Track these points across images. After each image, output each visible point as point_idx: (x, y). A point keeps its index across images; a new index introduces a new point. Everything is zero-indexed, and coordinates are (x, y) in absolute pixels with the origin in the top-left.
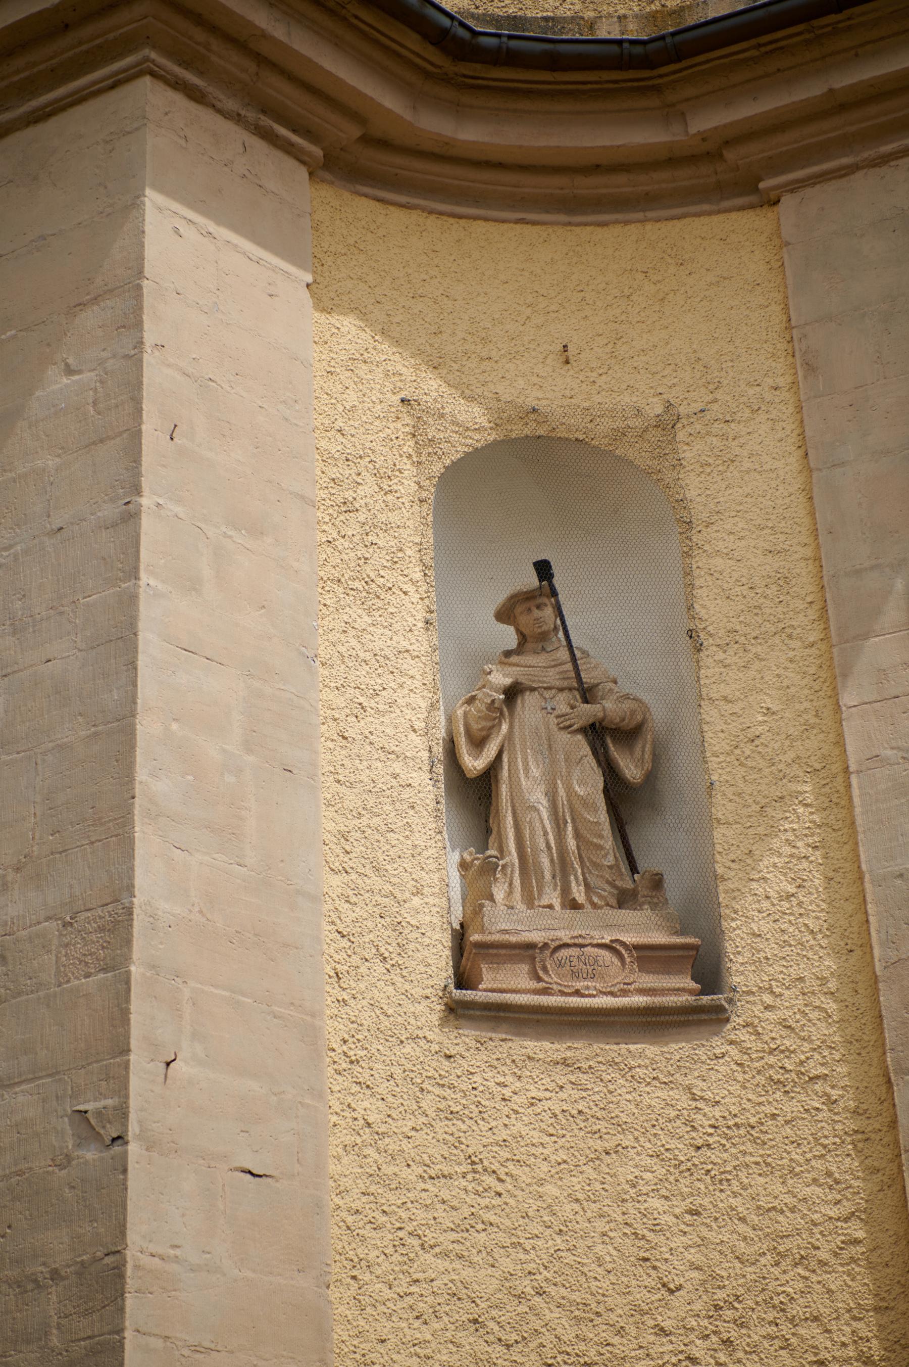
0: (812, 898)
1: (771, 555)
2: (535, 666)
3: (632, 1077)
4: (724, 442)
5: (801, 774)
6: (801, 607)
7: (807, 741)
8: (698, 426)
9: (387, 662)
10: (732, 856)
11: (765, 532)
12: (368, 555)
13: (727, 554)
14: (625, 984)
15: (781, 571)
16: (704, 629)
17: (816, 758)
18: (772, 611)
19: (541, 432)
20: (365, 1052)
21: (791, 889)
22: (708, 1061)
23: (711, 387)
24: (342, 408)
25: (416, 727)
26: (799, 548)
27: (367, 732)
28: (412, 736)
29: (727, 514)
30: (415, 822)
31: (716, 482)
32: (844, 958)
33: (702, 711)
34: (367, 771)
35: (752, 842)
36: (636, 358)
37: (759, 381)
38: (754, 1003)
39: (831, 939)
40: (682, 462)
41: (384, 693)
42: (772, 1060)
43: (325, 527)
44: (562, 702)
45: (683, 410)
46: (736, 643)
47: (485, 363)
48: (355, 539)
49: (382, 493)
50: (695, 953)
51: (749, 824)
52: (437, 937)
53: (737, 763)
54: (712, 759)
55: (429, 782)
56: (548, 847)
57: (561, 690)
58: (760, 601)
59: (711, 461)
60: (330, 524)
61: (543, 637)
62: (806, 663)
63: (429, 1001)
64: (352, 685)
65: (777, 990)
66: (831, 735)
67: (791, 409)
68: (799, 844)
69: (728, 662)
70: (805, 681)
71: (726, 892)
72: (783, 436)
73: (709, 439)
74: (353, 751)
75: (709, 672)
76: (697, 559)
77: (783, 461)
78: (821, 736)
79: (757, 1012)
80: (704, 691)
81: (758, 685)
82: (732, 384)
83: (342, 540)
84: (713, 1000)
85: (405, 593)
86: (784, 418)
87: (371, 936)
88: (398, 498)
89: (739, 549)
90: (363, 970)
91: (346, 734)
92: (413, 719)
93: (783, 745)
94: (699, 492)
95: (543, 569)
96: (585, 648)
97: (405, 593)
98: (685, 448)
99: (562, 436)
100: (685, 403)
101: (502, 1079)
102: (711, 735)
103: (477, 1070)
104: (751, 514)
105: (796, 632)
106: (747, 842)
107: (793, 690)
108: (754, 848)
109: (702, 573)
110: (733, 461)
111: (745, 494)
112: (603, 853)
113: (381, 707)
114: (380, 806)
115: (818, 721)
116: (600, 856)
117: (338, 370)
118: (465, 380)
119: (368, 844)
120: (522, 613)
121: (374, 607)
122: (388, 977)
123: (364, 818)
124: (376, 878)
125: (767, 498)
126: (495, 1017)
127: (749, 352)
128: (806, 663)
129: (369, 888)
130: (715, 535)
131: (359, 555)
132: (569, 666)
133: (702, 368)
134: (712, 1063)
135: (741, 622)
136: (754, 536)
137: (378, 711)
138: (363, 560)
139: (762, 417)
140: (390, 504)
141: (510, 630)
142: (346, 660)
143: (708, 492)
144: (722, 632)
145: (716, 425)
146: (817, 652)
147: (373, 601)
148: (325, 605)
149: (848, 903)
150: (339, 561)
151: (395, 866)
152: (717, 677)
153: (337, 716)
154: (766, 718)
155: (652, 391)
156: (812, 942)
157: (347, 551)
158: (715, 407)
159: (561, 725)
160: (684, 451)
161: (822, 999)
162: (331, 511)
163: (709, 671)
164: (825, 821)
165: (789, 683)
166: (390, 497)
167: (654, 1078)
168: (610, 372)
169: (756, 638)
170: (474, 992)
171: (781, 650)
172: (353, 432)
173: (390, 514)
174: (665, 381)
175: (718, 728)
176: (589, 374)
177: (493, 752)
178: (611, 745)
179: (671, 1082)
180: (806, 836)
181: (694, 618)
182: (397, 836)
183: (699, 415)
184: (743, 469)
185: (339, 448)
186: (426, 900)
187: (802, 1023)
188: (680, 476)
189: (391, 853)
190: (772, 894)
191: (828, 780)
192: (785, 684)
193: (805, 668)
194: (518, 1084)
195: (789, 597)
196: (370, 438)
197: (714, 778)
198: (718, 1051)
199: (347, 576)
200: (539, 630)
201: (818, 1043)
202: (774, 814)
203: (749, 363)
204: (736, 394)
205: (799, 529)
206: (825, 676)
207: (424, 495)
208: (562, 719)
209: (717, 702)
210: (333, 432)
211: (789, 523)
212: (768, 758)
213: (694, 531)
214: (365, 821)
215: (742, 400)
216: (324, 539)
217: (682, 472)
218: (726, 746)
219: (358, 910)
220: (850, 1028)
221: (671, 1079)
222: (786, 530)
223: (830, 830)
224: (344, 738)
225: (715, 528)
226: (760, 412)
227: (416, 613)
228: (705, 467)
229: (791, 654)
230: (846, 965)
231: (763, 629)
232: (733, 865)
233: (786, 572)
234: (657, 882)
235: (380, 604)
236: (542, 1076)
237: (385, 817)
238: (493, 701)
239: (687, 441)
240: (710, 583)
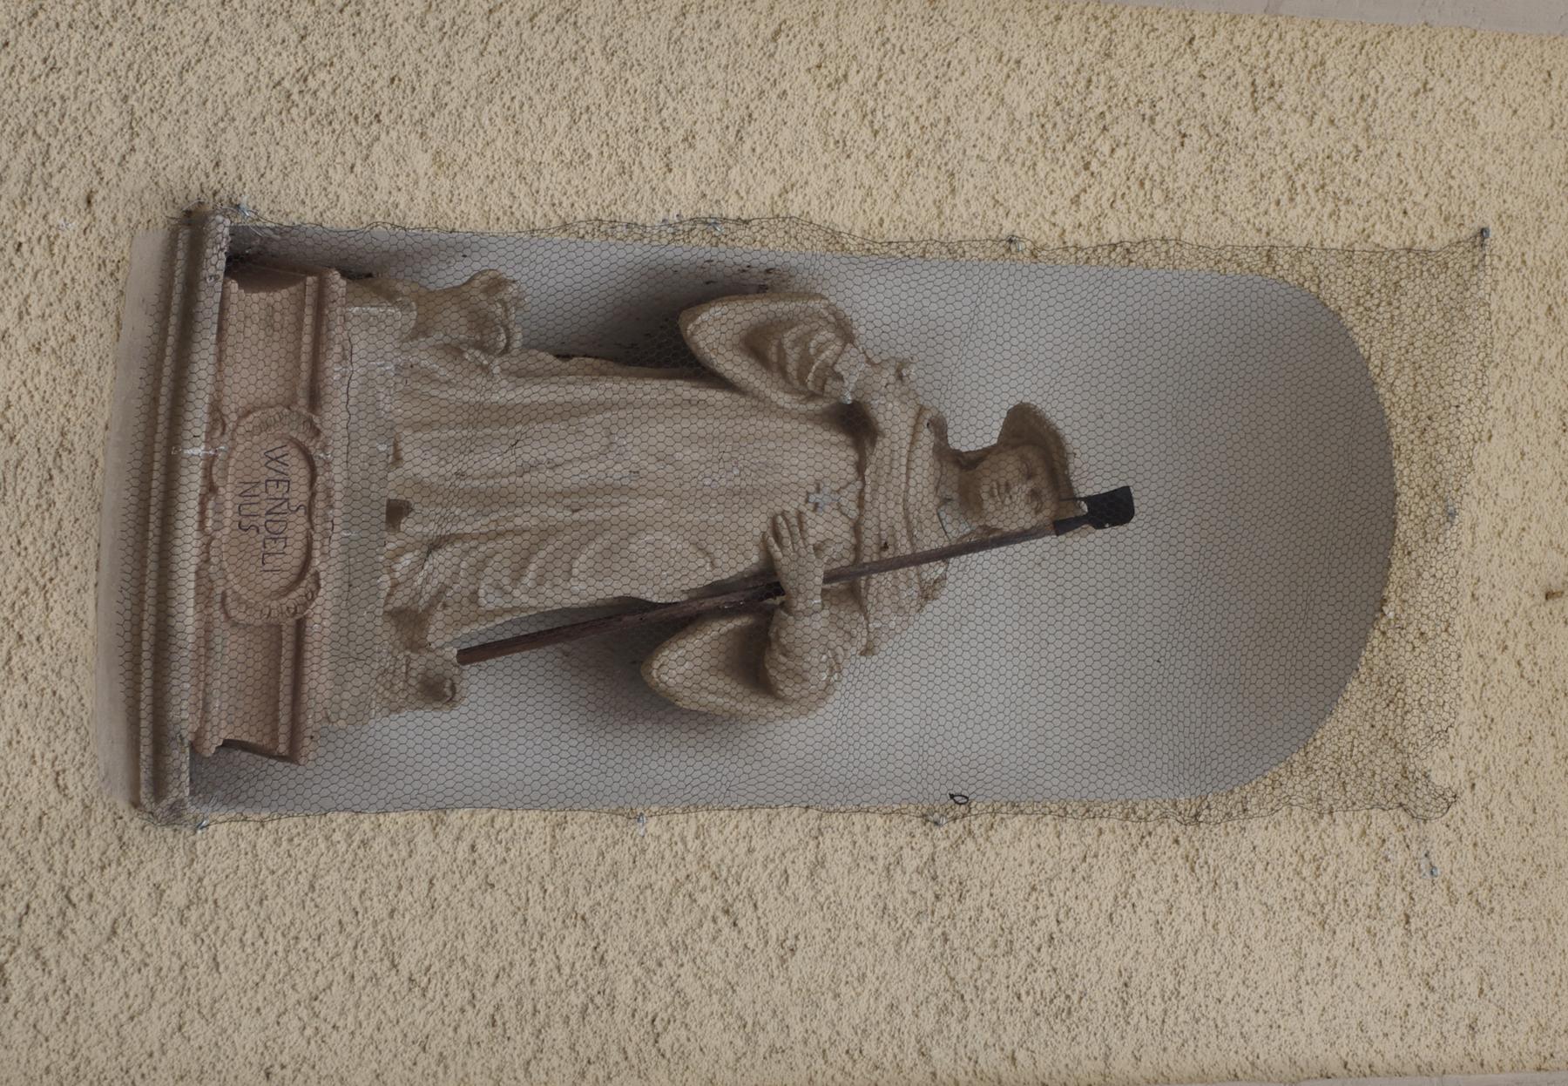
0: (387, 1006)
1: (1120, 985)
2: (907, 482)
3: (26, 592)
4: (1364, 911)
5: (650, 1007)
6: (1005, 1038)
7: (720, 1025)
8: (1400, 859)
9: (932, 145)
10: (483, 846)
11: (1170, 978)
12: (1159, 125)
13: (1126, 894)
14: (224, 595)
15: (1084, 1003)
16: (970, 832)
17: (683, 1040)
18: (1000, 976)
19: (1405, 526)
20: (107, 14)
21: (407, 963)
22: (49, 756)
23: (1483, 894)
24: (1472, 97)
25: (791, 196)
26: (1130, 1043)
27: (785, 85)
28: (773, 186)
29: (1211, 902)
30: (589, 175)
31: (1280, 885)
32: (255, 1059)
33: (796, 811)
34: (703, 80)
35: (512, 890)
36: (1552, 741)
37: (1490, 994)
38: (169, 864)
39: (296, 1034)
40: (1327, 818)
41: (866, 133)
42: (47, 888)
43: (1222, 33)
44: (829, 529)
45: (1436, 828)
46: (937, 897)
47: (1554, 418)
48: (1194, 99)
49: (1290, 168)
50: (282, 749)
51: (550, 889)
52: (344, 196)
53: (681, 875)
54: (693, 822)
55: (674, 212)
56: (525, 470)
57: (856, 529)
58: (1023, 953)
59: (1325, 878)
60: (1228, 46)
61: (968, 500)
62: (886, 1038)
63: (210, 166)
64: (887, 64)
65: (193, 915)
66: (729, 1073)
67: (1427, 1055)
68: (502, 990)
69: (898, 875)
70: (847, 1032)
71: (408, 827)
72: (1371, 1034)
73: (1372, 879)
74: (747, 52)
75: (877, 835)
76: (1119, 831)
77: (1317, 1028)
78: (729, 1056)
79: (149, 866)
80: (838, 821)
81: (844, 933)
82: (1488, 937)
83: (1194, 69)
84: (180, 772)
85: (1076, 200)
86: (1409, 1040)
87: (353, 54)
88: (1278, 203)
89: (1135, 920)
90: (282, 28)
91: (782, 39)
92: (808, 190)
93: (716, 974)
94: (1261, 849)
95: (1113, 509)
96: (945, 595)
97: (1076, 200)
98: (1357, 828)
99: (1394, 568)
100: (1451, 836)
101: (35, 311)
102: (743, 828)
103: (58, 260)
104: (1209, 952)
105: (953, 1022)
106: (513, 881)
107: (830, 1005)
108: (499, 894)
109: (1089, 840)
110: (1323, 924)
111: (1253, 945)
112: (506, 581)
113: (837, 125)
114: (627, 100)
115: (762, 1050)
116: (498, 576)
117: (1554, 94)
118: (1520, 370)
119: (548, 65)
120: (1023, 458)
121: (1049, 126)
122: (264, 80)
123: (602, 63)
124: (474, 78)
125: (1241, 989)
126: (168, 308)
127: (1553, 980)
128: (886, 1038)
129: (455, 58)
130: (1168, 872)
131: (1159, 104)
132: (905, 549)
133: (1522, 878)
134: (47, 765)
135: (980, 910)
136: (1161, 954)
137: (828, 114)
138: (1149, 112)
139: (1414, 995)
140: (1265, 185)
141: (989, 435)
142: (940, 55)
143: (1259, 867)
144: (962, 870)
145: (1400, 896)
146: (908, 1063)
147: (1061, 127)
148: (1058, 18)
149: (372, 1077)
150: (1150, 59)
151: (499, 121)
152: (867, 849)
153: (823, 22)
154: (772, 942)
155: (1480, 769)
156: (293, 998)
157: (1169, 78)
158: (1440, 898)
159: (780, 519)
160: (1348, 825)
161: (170, 1006)
162: (1256, 50)
163: (881, 835)
164: (547, 1045)
165: (846, 999)
166: (1279, 182)
167: (21, 637)
168: (1525, 683)
169: (945, 938)
170: (221, 274)
171: (916, 987)
172: (1422, 115)
173: (1245, 181)
174: (1501, 798)
175: (757, 843)
176: (1522, 641)
177: (728, 366)
178: (731, 626)
179: (11, 671)
180: (519, 1003)
181: (994, 813)
182: (561, 130)
183: (1424, 864)
184: (1305, 944)
185: (1389, 81)
186: (423, 183)
187: (120, 957)
188: (1297, 810)
189: (526, 115)
190: (399, 923)
191: (635, 1061)
192: (843, 989)
193: (875, 1034)
194: (22, 345)
195: (1027, 1014)
196: (1408, 152)
197: (652, 825)
198: (70, 779)
199: (1117, 72)
200: (985, 496)
201: (76, 989)
202: (567, 941)
203: (1529, 976)
204: (1464, 944)
205: (1172, 1048)
206: (857, 1074)
207: (1283, 260)
208: (794, 521)
209: (812, 844)
210: (1422, 73)
211: (1185, 1028)
212: (688, 941)
213: (1178, 829)
214: (598, 63)
215: (1451, 954)
216: (1196, 29)
217: (1306, 816)
218: (718, 856)
219: (410, 29)
220: (103, 1057)
221: (17, 673)
222: (1170, 1022)
223: (529, 1054)
224: (777, 33)
225: (1182, 874)
226: (1425, 991)
227: (1032, 217)
228: (1313, 866)
229: (908, 1009)
230: (239, 1060)
231: (963, 955)
232: (464, 846)
233: (1083, 1013)
234: (437, 692)
235: (1056, 139)
236: (37, 398)
237: (604, 109)
238: (840, 378)
239: (1371, 832)
240: (1065, 854)
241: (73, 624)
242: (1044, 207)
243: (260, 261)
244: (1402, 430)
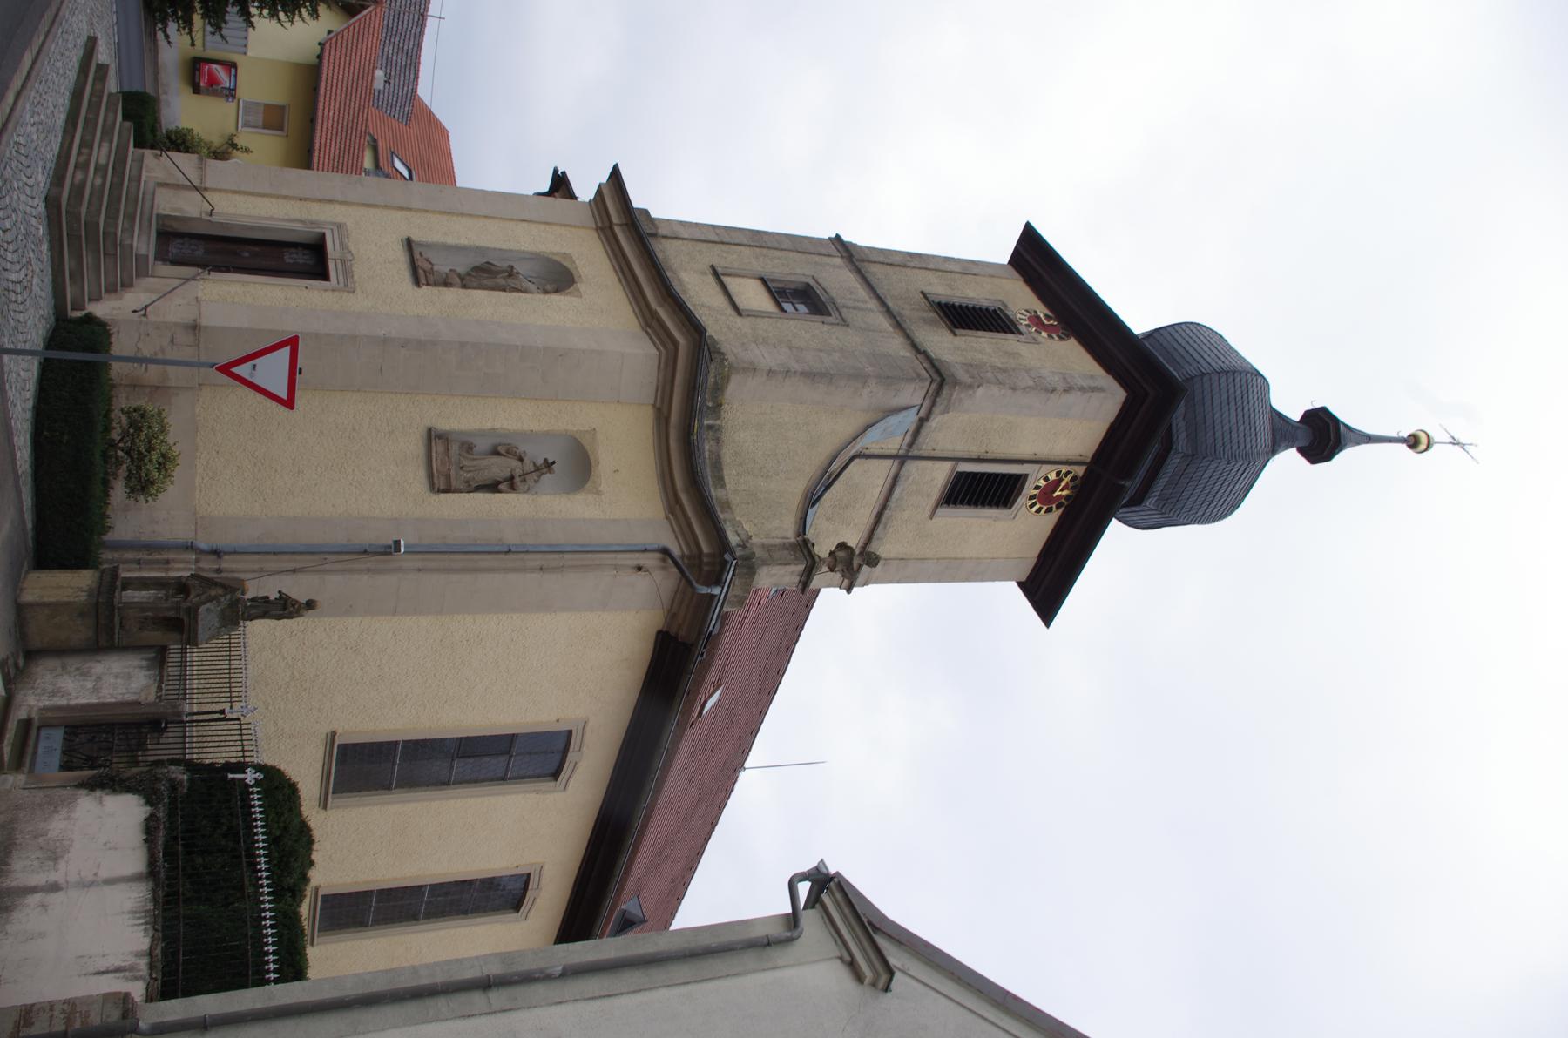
44: (518, 472)
241: (422, 473)
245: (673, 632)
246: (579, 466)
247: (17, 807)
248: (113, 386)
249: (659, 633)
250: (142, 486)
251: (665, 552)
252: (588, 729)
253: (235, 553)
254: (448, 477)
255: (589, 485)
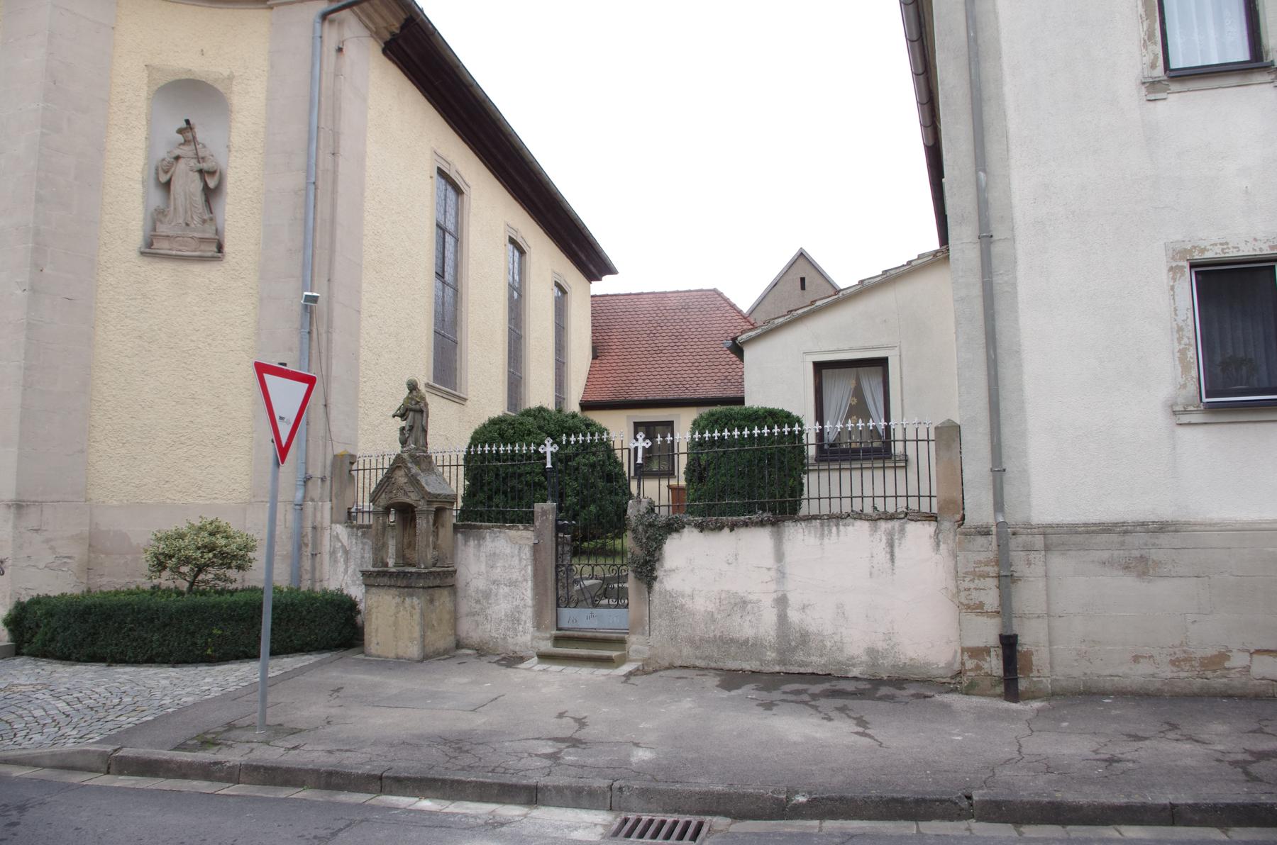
44: (193, 163)
95: (188, 122)
241: (198, 268)
242: (141, 133)
243: (150, 244)
244: (177, 78)
245: (388, 37)
246: (192, 96)
247: (673, 639)
248: (89, 591)
249: (384, 52)
250: (235, 559)
251: (324, 16)
252: (439, 151)
253: (306, 463)
254: (202, 240)
255: (220, 87)
